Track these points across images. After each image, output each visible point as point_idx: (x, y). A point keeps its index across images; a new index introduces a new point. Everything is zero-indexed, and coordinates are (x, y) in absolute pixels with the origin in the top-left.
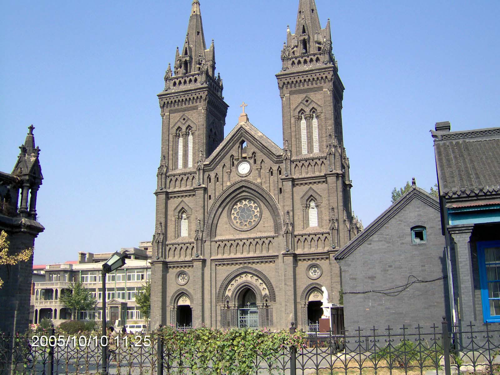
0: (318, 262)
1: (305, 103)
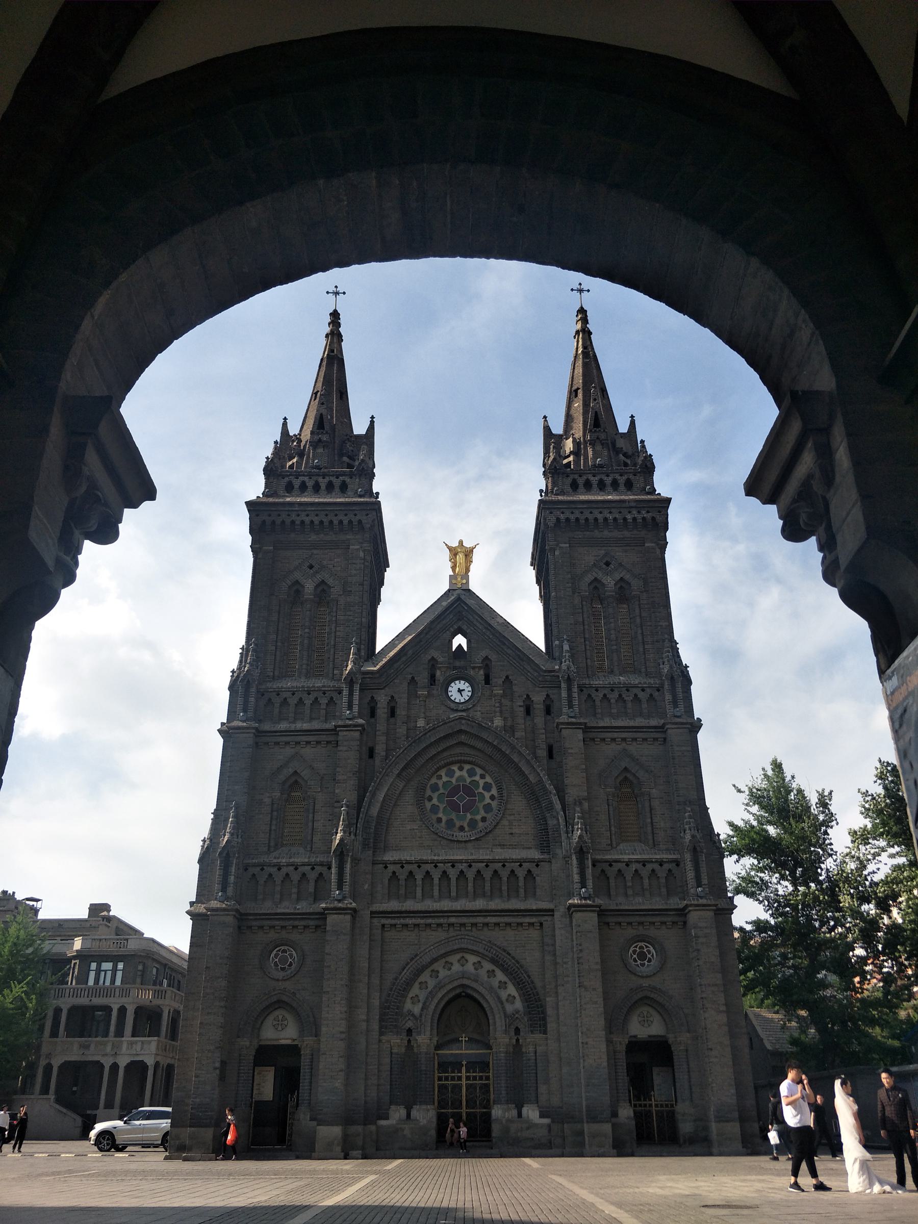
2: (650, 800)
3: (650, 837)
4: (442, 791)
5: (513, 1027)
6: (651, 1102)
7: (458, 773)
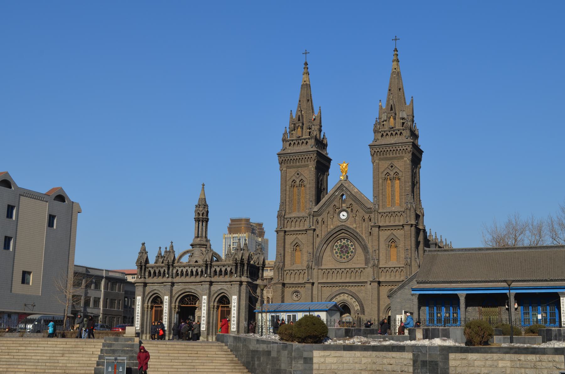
1: (390, 168)
4: (338, 247)
7: (343, 241)
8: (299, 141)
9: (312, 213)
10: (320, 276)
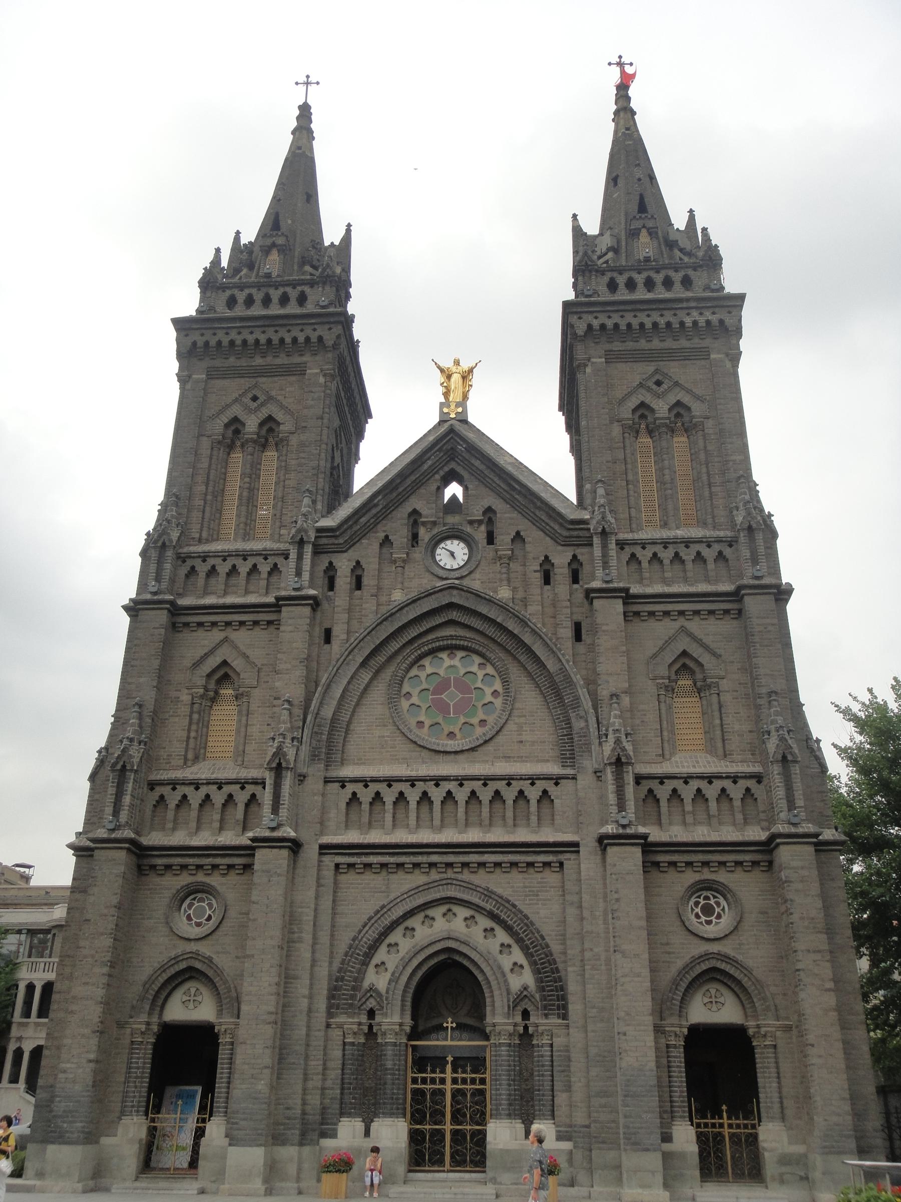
0: (722, 876)
2: (718, 694)
3: (719, 744)
4: (424, 686)
5: (520, 1009)
6: (721, 1121)
8: (272, 291)
9: (312, 535)
10: (336, 813)
